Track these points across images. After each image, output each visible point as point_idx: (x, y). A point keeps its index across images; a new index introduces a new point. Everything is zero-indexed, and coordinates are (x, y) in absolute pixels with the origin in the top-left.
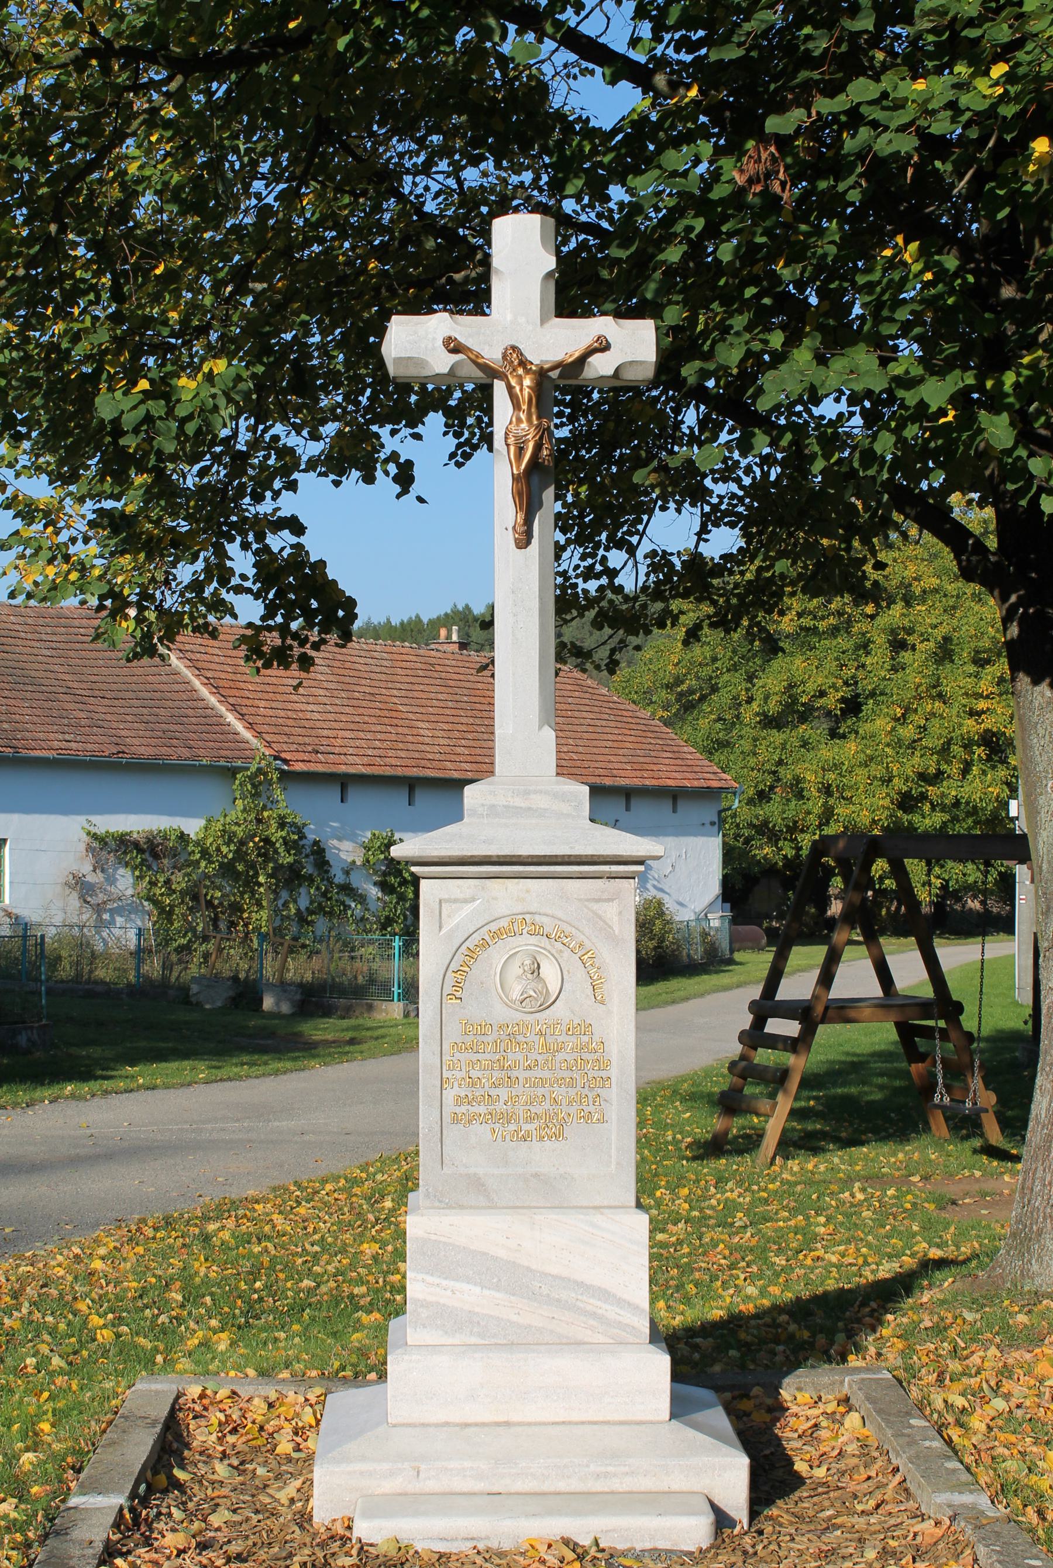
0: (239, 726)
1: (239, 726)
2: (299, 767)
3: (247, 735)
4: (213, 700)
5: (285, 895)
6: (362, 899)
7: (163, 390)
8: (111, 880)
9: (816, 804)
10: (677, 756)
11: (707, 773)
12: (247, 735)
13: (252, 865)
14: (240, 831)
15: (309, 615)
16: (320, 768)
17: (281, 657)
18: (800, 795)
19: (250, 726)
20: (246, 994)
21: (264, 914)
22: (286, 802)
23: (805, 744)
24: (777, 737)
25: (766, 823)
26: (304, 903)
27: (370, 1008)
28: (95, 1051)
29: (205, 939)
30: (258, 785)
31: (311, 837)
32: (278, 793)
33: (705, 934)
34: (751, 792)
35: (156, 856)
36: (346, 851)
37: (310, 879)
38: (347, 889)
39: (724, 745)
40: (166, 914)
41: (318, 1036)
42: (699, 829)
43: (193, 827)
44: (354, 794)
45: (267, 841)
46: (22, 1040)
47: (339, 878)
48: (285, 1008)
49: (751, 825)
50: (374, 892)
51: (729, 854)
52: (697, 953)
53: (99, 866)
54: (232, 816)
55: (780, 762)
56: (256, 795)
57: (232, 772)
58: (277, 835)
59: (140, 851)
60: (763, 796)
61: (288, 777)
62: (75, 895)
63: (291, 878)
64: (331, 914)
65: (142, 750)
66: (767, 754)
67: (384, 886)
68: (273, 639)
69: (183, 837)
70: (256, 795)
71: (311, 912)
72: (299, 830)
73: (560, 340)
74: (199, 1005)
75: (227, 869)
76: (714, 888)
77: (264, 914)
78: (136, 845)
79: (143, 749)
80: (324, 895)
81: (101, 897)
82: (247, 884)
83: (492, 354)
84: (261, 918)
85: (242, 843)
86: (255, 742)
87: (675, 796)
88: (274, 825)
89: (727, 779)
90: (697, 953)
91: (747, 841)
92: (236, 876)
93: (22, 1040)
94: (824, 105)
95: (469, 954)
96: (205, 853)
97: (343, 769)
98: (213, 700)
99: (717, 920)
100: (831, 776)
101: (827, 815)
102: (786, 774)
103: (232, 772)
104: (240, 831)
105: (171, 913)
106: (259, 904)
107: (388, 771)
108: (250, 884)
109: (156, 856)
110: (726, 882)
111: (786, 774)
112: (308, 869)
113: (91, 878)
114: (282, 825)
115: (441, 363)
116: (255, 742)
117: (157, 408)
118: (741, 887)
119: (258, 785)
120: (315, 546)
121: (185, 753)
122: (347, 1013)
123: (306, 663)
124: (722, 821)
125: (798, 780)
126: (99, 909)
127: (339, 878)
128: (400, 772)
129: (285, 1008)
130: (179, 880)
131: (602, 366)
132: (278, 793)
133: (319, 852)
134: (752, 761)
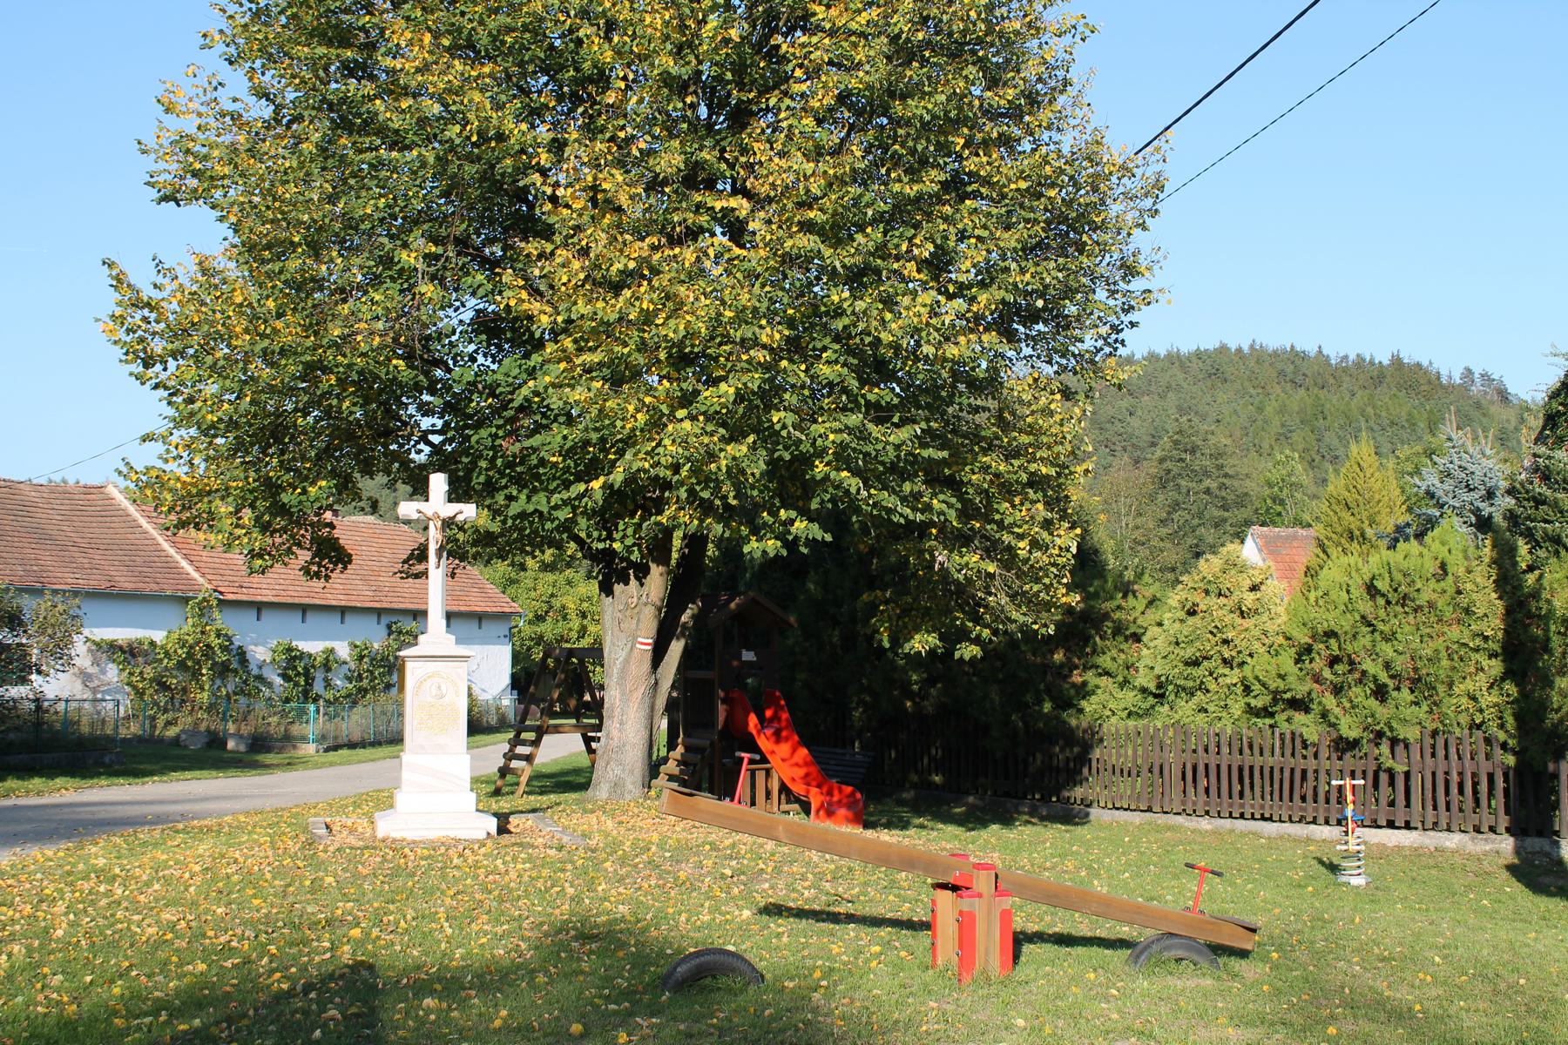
0: (190, 569)
1: (190, 569)
2: (230, 597)
3: (195, 575)
4: (172, 551)
5: (218, 682)
6: (270, 685)
7: (304, 492)
8: (104, 672)
9: (575, 624)
10: (482, 590)
11: (503, 604)
12: (195, 575)
13: (198, 662)
14: (191, 640)
15: (330, 558)
16: (244, 598)
17: (317, 575)
18: (565, 618)
19: (197, 569)
20: (216, 741)
21: (206, 695)
22: (221, 620)
23: (569, 583)
24: (550, 577)
25: (541, 637)
26: (231, 687)
27: (295, 747)
28: (148, 767)
29: (166, 711)
30: (203, 608)
31: (237, 644)
32: (216, 614)
33: (498, 709)
34: (531, 615)
35: (133, 656)
36: (260, 653)
37: (236, 671)
38: (260, 678)
39: (512, 582)
40: (140, 694)
41: (268, 761)
42: (496, 640)
43: (159, 636)
44: (265, 614)
45: (208, 646)
46: (107, 759)
47: (255, 671)
48: (242, 748)
49: (531, 639)
50: (278, 681)
51: (516, 658)
52: (493, 721)
53: (96, 662)
54: (186, 629)
55: (552, 595)
56: (201, 615)
57: (186, 600)
58: (215, 642)
59: (124, 652)
60: (540, 618)
61: (222, 603)
62: (79, 681)
63: (223, 670)
64: (249, 695)
65: (127, 585)
66: (544, 589)
67: (285, 677)
68: (315, 568)
69: (152, 643)
70: (201, 615)
71: (236, 694)
72: (229, 639)
73: (450, 510)
74: (186, 747)
75: (181, 665)
76: (507, 680)
77: (206, 695)
78: (121, 648)
79: (126, 584)
80: (245, 682)
81: (97, 683)
82: (194, 674)
83: (430, 514)
84: (204, 697)
85: (191, 647)
86: (201, 580)
87: (480, 617)
88: (213, 635)
89: (515, 607)
90: (493, 721)
91: (529, 649)
92: (186, 668)
93: (107, 759)
94: (527, 443)
95: (421, 683)
96: (167, 654)
97: (259, 598)
98: (172, 551)
99: (508, 702)
100: (585, 605)
101: (583, 632)
102: (557, 603)
103: (186, 600)
104: (191, 640)
105: (143, 693)
106: (202, 689)
107: (290, 600)
108: (196, 675)
109: (133, 656)
110: (513, 676)
111: (557, 603)
112: (234, 665)
113: (90, 670)
114: (218, 636)
115: (415, 516)
116: (201, 580)
117: (303, 498)
118: (524, 681)
119: (203, 608)
120: (336, 533)
121: (155, 587)
122: (281, 750)
123: (327, 578)
124: (512, 636)
125: (564, 607)
126: (94, 690)
127: (255, 671)
128: (297, 601)
129: (242, 748)
130: (149, 672)
131: (460, 518)
132: (216, 614)
133: (242, 654)
134: (533, 594)
